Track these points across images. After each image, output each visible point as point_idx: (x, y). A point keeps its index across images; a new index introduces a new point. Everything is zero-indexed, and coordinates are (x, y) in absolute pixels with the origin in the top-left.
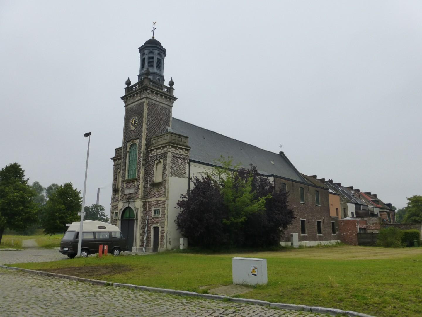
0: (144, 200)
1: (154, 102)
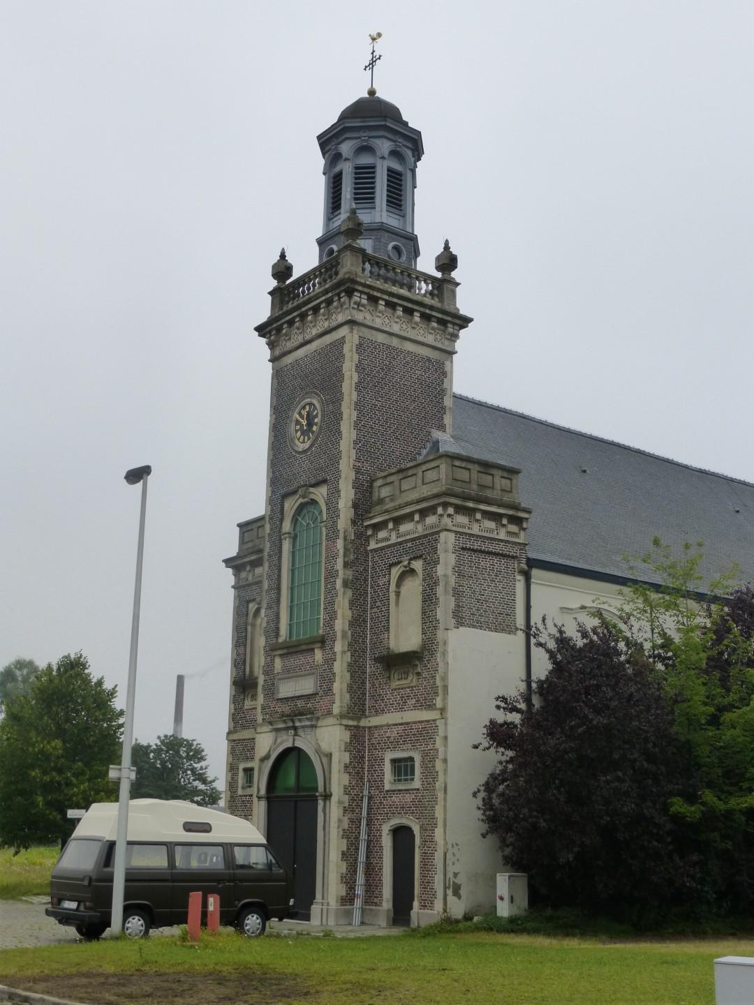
0: (351, 723)
1: (381, 338)
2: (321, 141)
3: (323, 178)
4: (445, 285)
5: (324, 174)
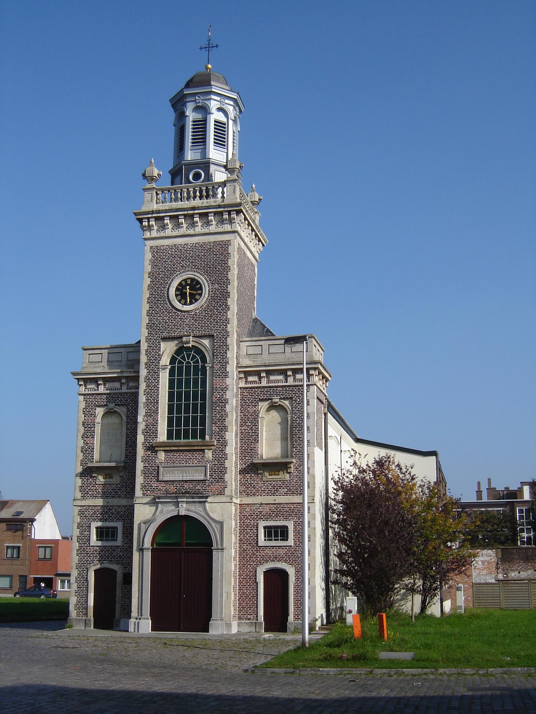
2: (172, 103)
3: (173, 128)
4: (257, 377)
5: (174, 125)
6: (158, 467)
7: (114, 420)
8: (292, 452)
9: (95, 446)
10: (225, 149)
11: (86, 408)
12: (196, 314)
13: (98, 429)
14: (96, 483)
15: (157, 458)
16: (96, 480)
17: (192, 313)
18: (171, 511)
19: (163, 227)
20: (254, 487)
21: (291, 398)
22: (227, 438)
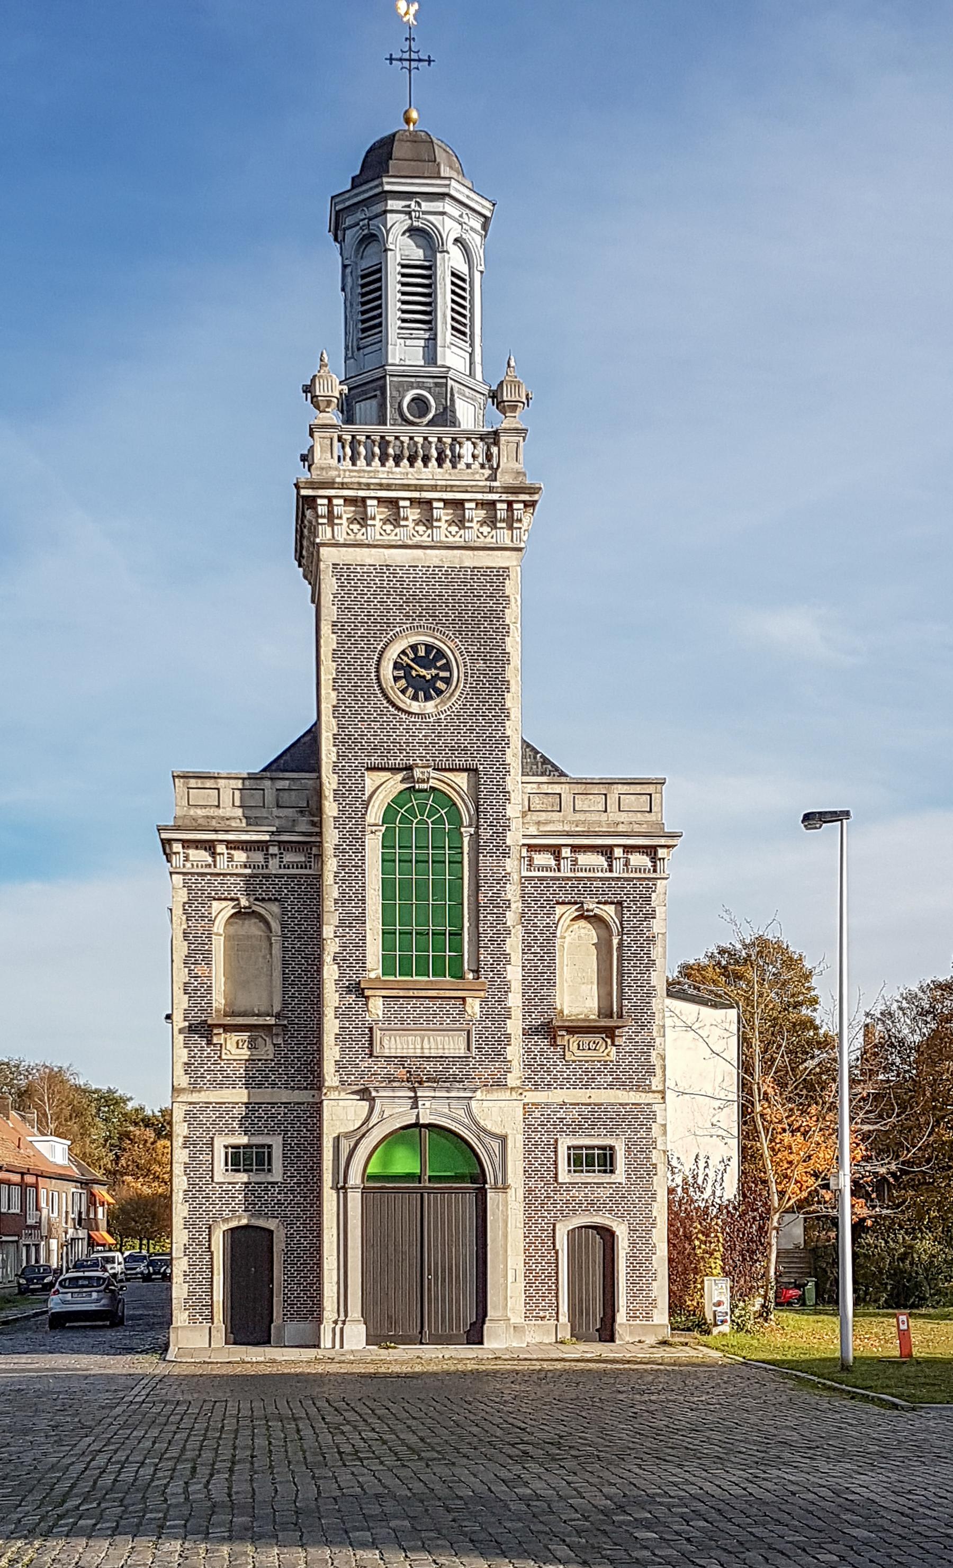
6: (371, 1029)
7: (253, 928)
8: (621, 1007)
9: (213, 982)
10: (466, 342)
11: (189, 902)
12: (438, 721)
13: (218, 946)
14: (220, 1057)
15: (368, 1011)
16: (220, 1050)
17: (432, 720)
18: (401, 1114)
19: (361, 521)
20: (549, 1072)
21: (620, 903)
22: (509, 978)
